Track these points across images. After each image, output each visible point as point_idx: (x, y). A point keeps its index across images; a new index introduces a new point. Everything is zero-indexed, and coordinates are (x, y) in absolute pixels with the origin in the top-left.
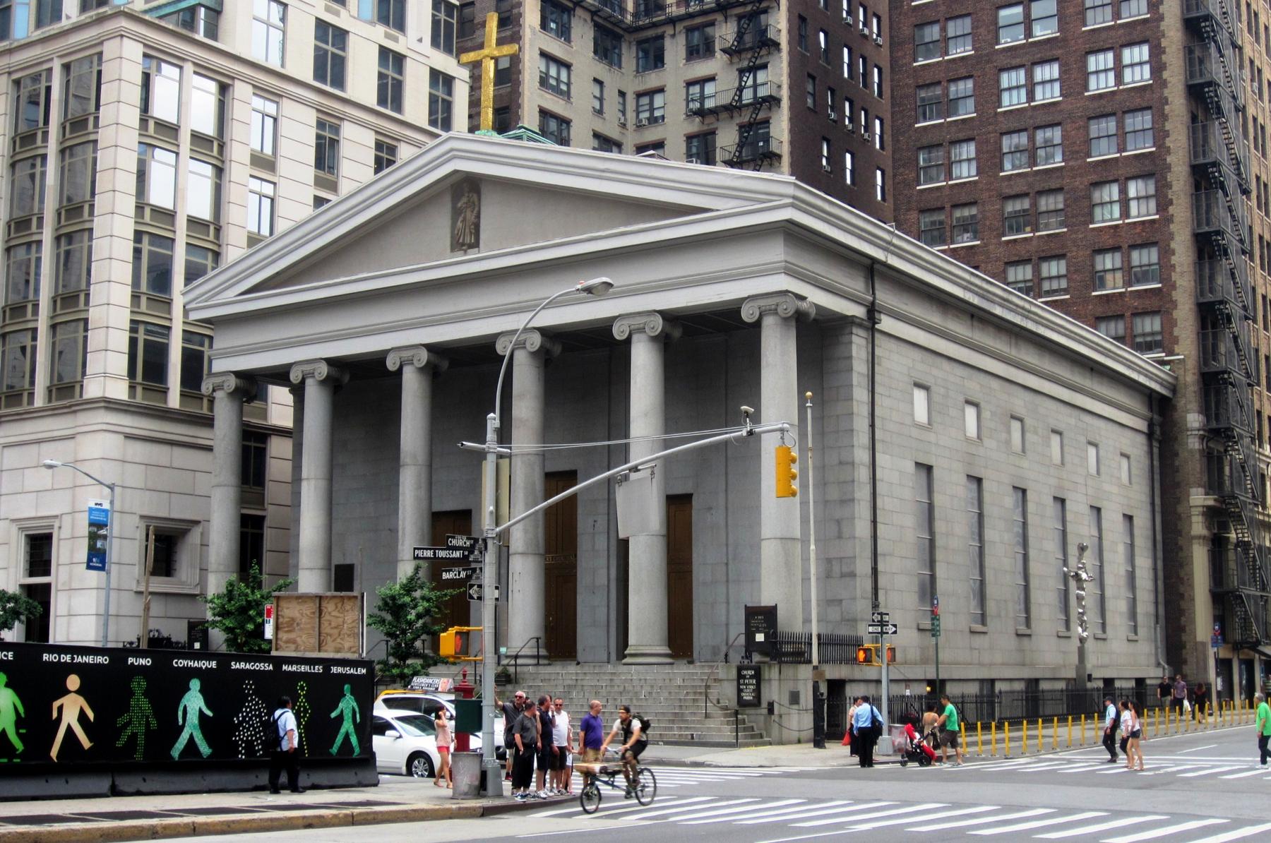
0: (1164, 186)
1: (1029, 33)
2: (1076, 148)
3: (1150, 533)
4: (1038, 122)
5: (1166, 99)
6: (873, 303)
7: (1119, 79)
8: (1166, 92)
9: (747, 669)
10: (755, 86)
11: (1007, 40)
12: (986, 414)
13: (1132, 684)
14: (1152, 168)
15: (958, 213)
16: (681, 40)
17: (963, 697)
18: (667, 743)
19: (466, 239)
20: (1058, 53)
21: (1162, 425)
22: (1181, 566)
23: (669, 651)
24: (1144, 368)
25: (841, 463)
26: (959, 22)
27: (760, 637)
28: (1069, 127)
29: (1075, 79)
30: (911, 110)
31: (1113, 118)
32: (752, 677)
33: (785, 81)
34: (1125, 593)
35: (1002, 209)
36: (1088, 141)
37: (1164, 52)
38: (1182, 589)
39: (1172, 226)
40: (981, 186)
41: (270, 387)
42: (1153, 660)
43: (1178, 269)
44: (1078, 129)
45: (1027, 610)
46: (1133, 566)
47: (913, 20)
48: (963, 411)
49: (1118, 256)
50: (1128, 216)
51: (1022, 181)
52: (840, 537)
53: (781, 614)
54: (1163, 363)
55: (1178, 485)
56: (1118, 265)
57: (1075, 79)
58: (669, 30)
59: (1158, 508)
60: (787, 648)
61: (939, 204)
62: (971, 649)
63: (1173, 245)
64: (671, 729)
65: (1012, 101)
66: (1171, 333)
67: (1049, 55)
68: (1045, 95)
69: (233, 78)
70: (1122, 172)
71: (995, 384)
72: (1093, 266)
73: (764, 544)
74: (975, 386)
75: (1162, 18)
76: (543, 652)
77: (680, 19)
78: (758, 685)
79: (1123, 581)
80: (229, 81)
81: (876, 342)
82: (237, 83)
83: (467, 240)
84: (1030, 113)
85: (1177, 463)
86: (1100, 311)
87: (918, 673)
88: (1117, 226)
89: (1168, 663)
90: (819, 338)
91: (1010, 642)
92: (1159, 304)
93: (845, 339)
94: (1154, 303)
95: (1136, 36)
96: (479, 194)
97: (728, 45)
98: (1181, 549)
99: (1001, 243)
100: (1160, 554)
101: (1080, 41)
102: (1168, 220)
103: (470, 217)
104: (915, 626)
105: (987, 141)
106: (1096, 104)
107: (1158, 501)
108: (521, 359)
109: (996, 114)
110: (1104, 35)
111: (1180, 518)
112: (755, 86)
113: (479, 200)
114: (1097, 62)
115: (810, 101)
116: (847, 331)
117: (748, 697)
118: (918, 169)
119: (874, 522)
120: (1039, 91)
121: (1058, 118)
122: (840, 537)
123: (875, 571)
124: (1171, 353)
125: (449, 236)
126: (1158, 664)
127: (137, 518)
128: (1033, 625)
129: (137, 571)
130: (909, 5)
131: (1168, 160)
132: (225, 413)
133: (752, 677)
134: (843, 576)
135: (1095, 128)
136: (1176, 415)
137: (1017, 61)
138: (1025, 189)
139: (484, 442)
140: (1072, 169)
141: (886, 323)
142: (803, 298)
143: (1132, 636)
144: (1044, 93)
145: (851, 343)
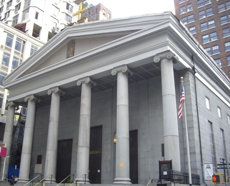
2: (225, 63)
20: (218, 43)
23: (130, 180)
27: (165, 173)
44: (224, 59)
60: (176, 178)
67: (216, 44)
69: (27, 40)
76: (87, 179)
80: (26, 41)
82: (27, 41)
90: (180, 73)
96: (75, 43)
103: (72, 49)
108: (84, 86)
113: (75, 45)
116: (187, 73)
123: (201, 152)
142: (175, 55)
145: (189, 76)
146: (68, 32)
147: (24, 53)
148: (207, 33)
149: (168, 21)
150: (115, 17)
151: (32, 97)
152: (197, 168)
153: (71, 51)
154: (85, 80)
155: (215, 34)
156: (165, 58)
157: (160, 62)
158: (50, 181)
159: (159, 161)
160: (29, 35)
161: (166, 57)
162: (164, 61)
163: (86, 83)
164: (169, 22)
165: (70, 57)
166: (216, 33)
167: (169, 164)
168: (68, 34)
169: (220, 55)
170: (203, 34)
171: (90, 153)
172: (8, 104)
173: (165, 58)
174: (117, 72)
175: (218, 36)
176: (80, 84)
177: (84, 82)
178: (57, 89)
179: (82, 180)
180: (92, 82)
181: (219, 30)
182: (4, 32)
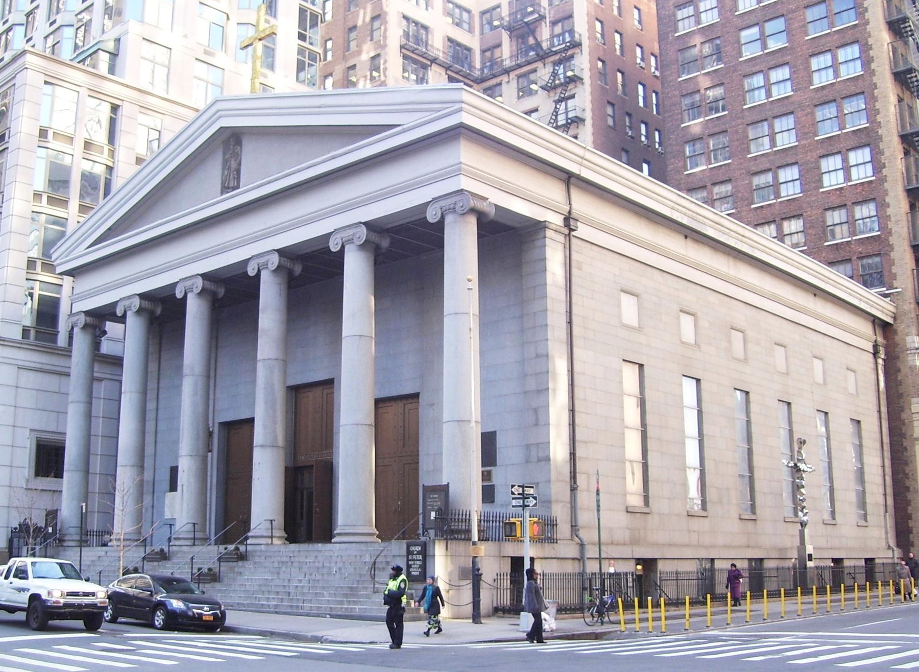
0: (877, 154)
1: (764, 46)
2: (806, 130)
3: (878, 436)
4: (776, 112)
5: (875, 85)
6: (570, 212)
7: (836, 74)
8: (875, 79)
9: (415, 545)
10: (567, 112)
11: (748, 53)
12: (704, 323)
13: (863, 563)
14: (867, 138)
15: (716, 189)
16: (514, 84)
17: (677, 573)
18: (332, 616)
19: (231, 183)
20: (787, 58)
21: (886, 347)
22: (906, 464)
24: (883, 309)
25: (537, 356)
26: (784, 119)
28: (799, 114)
29: (802, 77)
30: (677, 114)
31: (834, 104)
32: (419, 553)
33: (588, 106)
34: (854, 486)
35: (751, 183)
36: (815, 124)
37: (871, 49)
38: (908, 483)
39: (886, 184)
40: (732, 167)
41: (108, 323)
42: (883, 543)
43: (893, 219)
45: (753, 498)
46: (862, 464)
47: (677, 47)
48: (678, 318)
49: (843, 212)
50: (850, 180)
51: (764, 159)
52: (537, 425)
53: (451, 489)
54: (886, 296)
55: (901, 396)
56: (844, 219)
57: (802, 77)
58: (505, 78)
59: (884, 415)
61: (701, 184)
62: (689, 531)
63: (888, 200)
64: (342, 602)
65: (832, 181)
66: (890, 271)
67: (781, 61)
68: (779, 92)
70: (843, 145)
71: (713, 298)
72: (824, 221)
73: (445, 426)
74: (690, 297)
75: (867, 23)
77: (512, 69)
78: (424, 560)
79: (852, 477)
81: (573, 247)
83: (231, 185)
84: (768, 107)
85: (899, 378)
86: (832, 257)
87: (627, 552)
88: (842, 188)
89: (898, 546)
91: (735, 526)
92: (879, 246)
93: (538, 243)
94: (875, 248)
95: (848, 39)
97: (544, 83)
98: (906, 449)
99: (751, 210)
100: (887, 454)
101: (804, 48)
102: (882, 180)
103: (234, 164)
104: (624, 508)
105: (737, 132)
106: (819, 95)
107: (884, 409)
108: (265, 276)
109: (743, 110)
110: (823, 41)
111: (904, 424)
112: (567, 112)
114: (818, 63)
115: (610, 122)
116: (541, 235)
117: (415, 572)
118: (685, 158)
119: (572, 411)
120: (774, 89)
121: (791, 109)
122: (537, 425)
124: (891, 287)
125: (220, 182)
126: (889, 547)
127: (28, 432)
128: (758, 511)
129: (26, 472)
130: (673, 36)
131: (880, 132)
132: (81, 343)
133: (419, 553)
134: (539, 460)
135: (820, 114)
136: (897, 338)
137: (757, 68)
138: (768, 166)
139: (39, 295)
140: (804, 146)
141: (582, 231)
143: (863, 523)
144: (779, 91)
146: (220, 113)
147: (117, 146)
148: (753, 19)
149: (457, 106)
151: (137, 302)
152: (553, 499)
153: (232, 169)
155: (779, 24)
158: (268, 537)
160: (35, 253)
162: (449, 219)
164: (460, 110)
166: (782, 20)
167: (443, 494)
169: (791, 100)
170: (739, 23)
171: (331, 454)
172: (74, 319)
173: (453, 210)
175: (788, 31)
176: (256, 271)
177: (266, 265)
178: (199, 282)
179: (266, 534)
180: (288, 264)
181: (794, 11)
182: (46, 83)
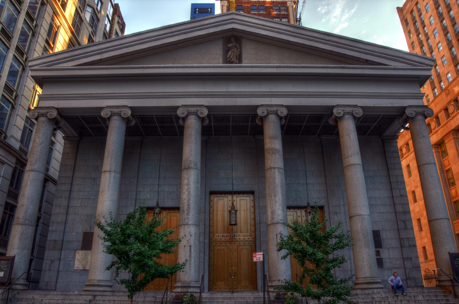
108: (272, 117)
146: (234, 21)
150: (303, 26)
154: (47, 112)
156: (118, 115)
157: (109, 119)
159: (449, 253)
161: (46, 115)
163: (123, 116)
165: (236, 63)
168: (233, 23)
174: (38, 115)
